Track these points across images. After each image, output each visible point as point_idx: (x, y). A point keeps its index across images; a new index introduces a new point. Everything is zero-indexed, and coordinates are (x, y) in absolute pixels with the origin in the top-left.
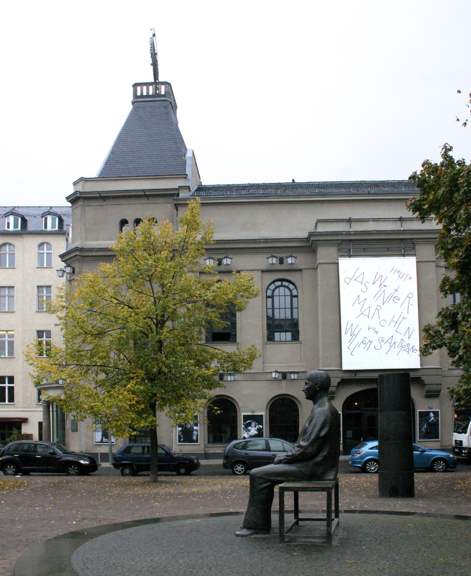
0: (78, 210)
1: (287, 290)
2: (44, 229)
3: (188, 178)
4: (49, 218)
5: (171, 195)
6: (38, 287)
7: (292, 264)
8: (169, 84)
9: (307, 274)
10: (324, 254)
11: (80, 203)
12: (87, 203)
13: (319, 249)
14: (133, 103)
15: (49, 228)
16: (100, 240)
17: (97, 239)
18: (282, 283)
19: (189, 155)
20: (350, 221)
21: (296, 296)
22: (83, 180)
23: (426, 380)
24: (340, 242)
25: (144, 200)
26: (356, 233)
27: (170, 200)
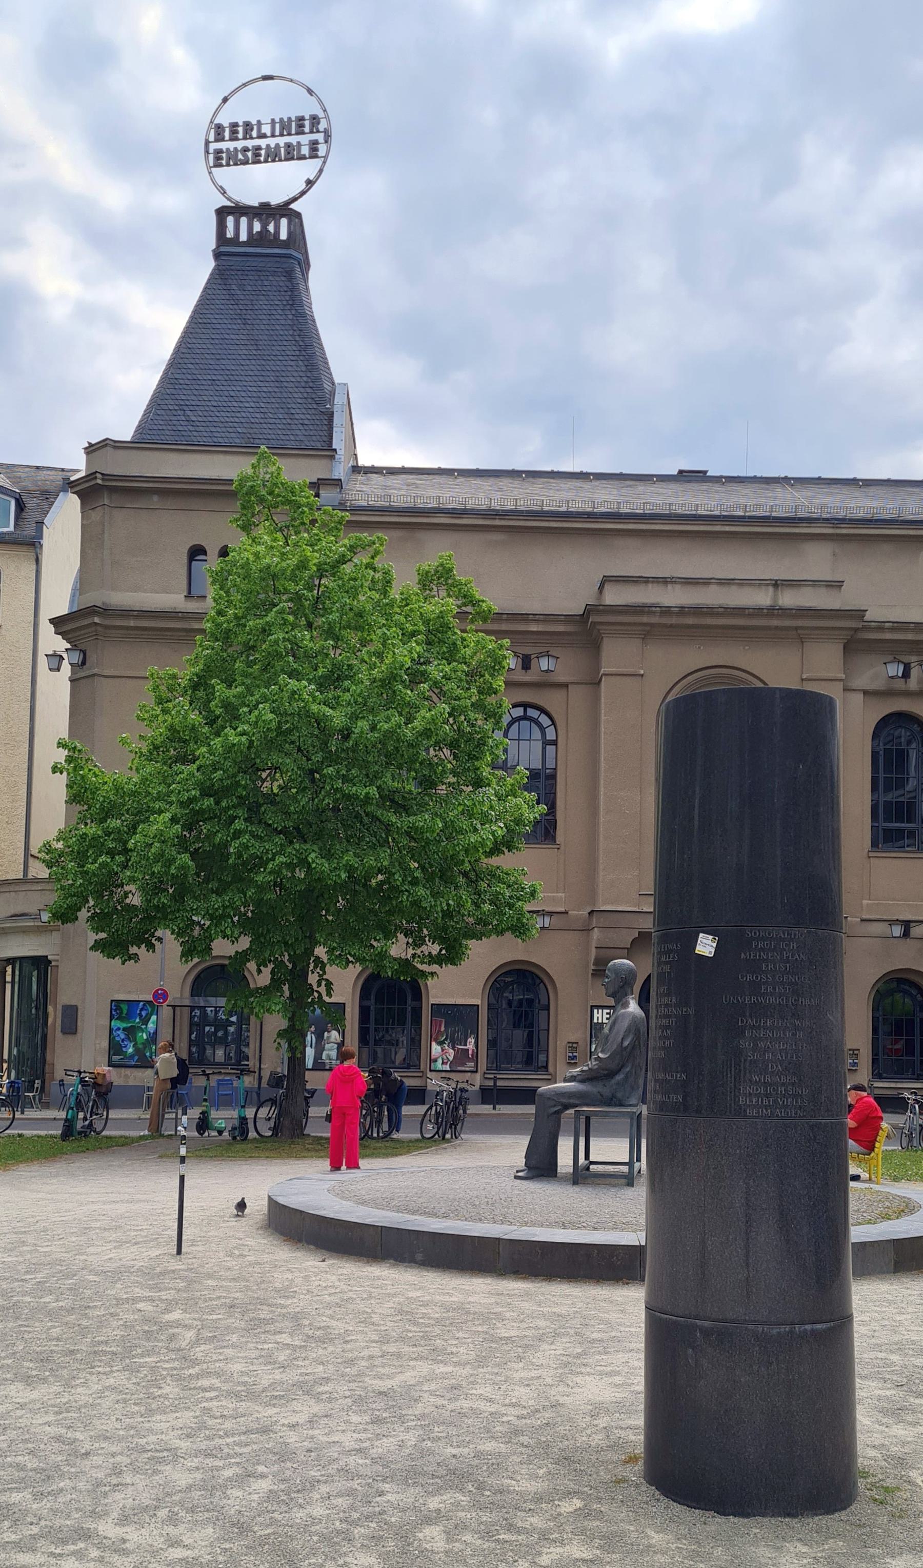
0: (95, 516)
1: (535, 729)
3: (337, 456)
7: (548, 671)
8: (298, 215)
9: (577, 694)
13: (605, 641)
14: (217, 255)
16: (145, 591)
17: (136, 589)
18: (525, 711)
19: (339, 399)
21: (554, 743)
24: (648, 628)
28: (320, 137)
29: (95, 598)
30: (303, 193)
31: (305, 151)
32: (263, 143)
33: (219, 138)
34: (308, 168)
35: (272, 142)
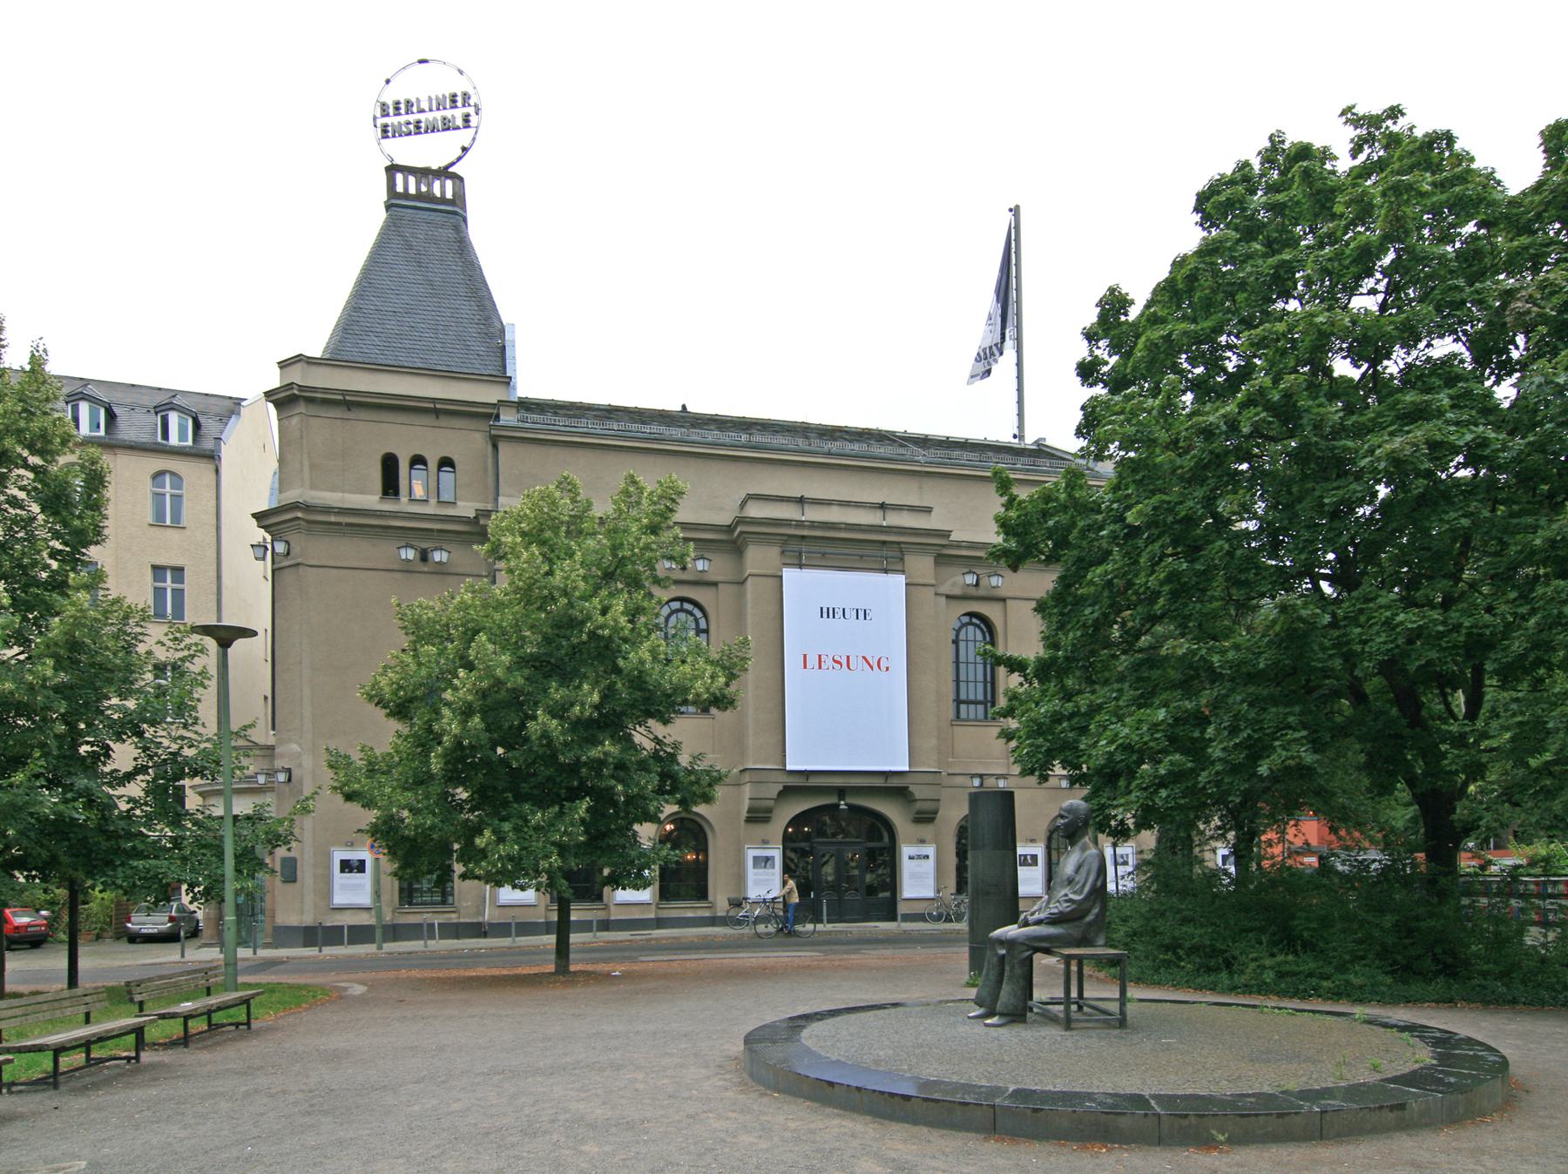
2: (159, 439)
4: (174, 418)
5: (485, 415)
6: (155, 568)
8: (461, 179)
10: (758, 557)
11: (301, 408)
12: (313, 410)
15: (174, 440)
20: (801, 501)
22: (299, 359)
23: (918, 792)
25: (429, 420)
26: (813, 525)
27: (483, 425)
28: (471, 110)
29: (292, 495)
30: (459, 159)
31: (459, 122)
32: (422, 117)
33: (385, 114)
34: (464, 137)
35: (430, 116)
